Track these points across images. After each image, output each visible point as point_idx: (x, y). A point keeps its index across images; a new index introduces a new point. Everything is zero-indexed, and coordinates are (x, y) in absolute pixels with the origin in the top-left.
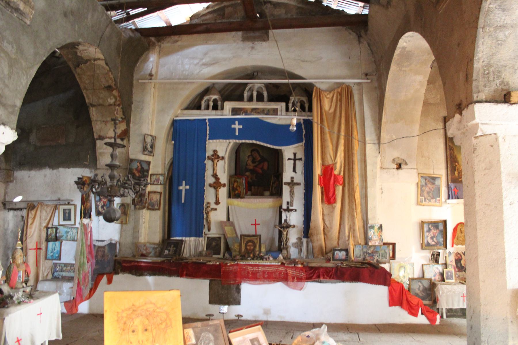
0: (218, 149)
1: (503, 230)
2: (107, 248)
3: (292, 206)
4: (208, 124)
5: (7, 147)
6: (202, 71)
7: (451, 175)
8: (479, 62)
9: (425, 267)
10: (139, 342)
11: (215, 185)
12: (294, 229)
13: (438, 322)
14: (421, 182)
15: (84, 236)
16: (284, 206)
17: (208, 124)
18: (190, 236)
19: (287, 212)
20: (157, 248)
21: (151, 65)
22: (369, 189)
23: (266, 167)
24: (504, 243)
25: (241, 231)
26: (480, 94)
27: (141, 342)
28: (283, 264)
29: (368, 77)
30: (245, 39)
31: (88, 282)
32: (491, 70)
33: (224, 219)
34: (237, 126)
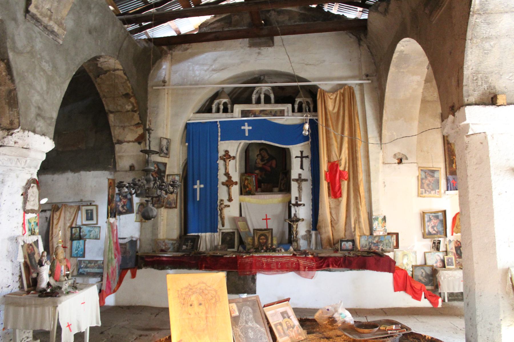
0: (229, 149)
1: (493, 217)
3: (301, 201)
4: (219, 126)
5: (48, 154)
9: (427, 255)
10: (195, 313)
11: (227, 183)
12: (303, 223)
13: (440, 305)
14: (421, 175)
16: (293, 201)
18: (206, 232)
19: (296, 207)
20: (175, 244)
21: (164, 73)
22: (372, 183)
23: (274, 165)
24: (494, 229)
25: (253, 226)
26: (470, 97)
28: (294, 255)
29: (368, 78)
30: (251, 45)
31: (115, 276)
32: (479, 76)
33: (238, 215)
34: (247, 128)
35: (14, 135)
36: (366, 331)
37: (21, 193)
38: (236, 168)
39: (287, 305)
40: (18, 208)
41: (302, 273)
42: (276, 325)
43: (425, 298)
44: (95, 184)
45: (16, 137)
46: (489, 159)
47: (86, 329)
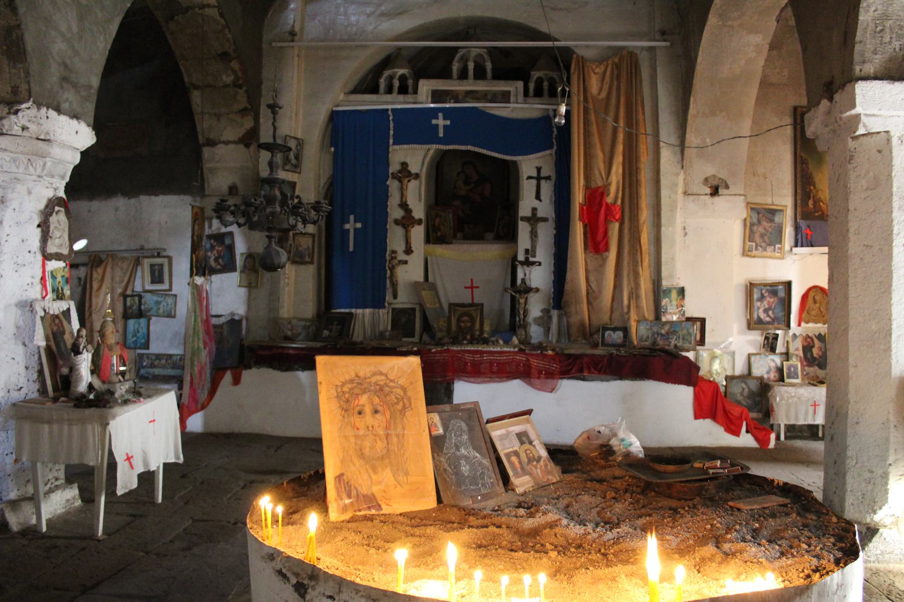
1: (890, 286)
2: (225, 327)
3: (534, 256)
4: (391, 118)
5: (84, 154)
6: (380, 27)
7: (802, 206)
8: (868, 11)
9: (753, 358)
10: (368, 427)
12: (537, 295)
13: (772, 444)
14: (751, 217)
15: (197, 303)
16: (521, 257)
17: (391, 118)
19: (525, 267)
20: (309, 326)
21: (292, 17)
22: (663, 229)
27: (371, 429)
28: (521, 350)
29: (665, 37)
32: (888, 24)
33: (421, 279)
34: (441, 122)
35: (20, 114)
36: (671, 468)
37: (37, 223)
38: (420, 195)
39: (528, 421)
40: (33, 251)
41: (537, 382)
42: (508, 455)
43: (747, 431)
44: (167, 217)
45: (25, 118)
46: (892, 182)
47: (158, 467)
